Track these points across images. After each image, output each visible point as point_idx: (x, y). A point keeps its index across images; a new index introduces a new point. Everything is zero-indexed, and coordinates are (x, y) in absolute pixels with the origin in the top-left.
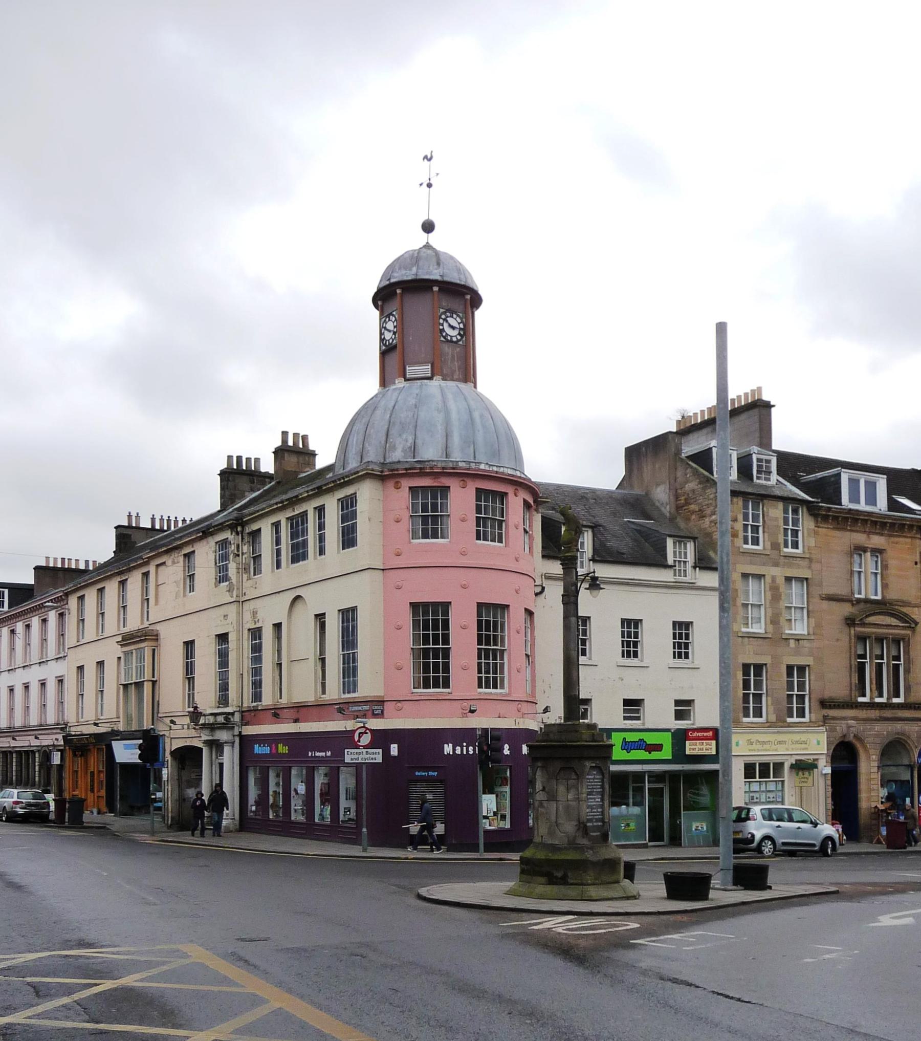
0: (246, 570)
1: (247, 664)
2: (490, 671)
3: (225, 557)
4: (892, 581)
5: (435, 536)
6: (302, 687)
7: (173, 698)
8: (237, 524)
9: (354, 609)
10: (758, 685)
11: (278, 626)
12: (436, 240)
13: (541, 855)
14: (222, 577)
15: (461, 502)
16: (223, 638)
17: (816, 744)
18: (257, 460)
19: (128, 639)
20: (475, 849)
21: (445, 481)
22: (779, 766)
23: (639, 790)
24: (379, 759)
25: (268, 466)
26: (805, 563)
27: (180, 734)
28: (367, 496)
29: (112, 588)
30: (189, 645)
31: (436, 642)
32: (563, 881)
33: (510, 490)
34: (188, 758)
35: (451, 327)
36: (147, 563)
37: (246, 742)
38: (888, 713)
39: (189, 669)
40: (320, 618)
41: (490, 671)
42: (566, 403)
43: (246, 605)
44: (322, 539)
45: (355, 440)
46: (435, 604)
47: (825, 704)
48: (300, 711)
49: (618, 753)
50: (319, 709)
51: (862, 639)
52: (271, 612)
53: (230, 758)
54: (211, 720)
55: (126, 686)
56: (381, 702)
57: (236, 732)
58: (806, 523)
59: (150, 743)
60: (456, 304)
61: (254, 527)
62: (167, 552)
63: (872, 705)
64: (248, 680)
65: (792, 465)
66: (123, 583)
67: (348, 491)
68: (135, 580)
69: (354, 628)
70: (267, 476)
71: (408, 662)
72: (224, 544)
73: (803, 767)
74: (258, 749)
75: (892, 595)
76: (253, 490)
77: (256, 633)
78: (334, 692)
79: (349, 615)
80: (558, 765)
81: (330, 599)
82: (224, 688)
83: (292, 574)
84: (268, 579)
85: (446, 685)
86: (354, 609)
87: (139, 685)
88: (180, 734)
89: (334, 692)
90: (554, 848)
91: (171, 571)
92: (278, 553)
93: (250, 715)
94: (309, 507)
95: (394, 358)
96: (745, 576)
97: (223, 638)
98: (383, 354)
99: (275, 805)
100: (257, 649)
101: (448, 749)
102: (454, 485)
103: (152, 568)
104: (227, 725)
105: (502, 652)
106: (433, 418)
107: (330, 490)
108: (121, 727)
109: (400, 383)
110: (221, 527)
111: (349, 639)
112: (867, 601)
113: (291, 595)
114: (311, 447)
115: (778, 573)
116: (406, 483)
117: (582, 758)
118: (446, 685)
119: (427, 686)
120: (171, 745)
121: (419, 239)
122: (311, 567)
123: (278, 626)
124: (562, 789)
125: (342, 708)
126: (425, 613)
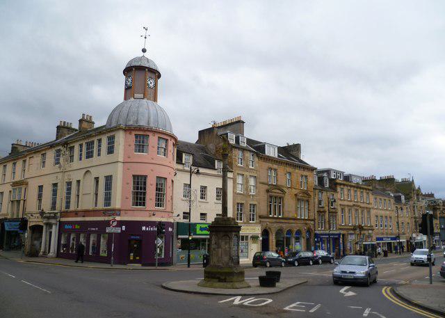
0: (67, 161)
1: (65, 195)
2: (159, 201)
3: (58, 156)
4: (279, 179)
5: (143, 152)
6: (87, 203)
7: (32, 206)
8: (65, 144)
9: (111, 176)
10: (241, 210)
11: (78, 182)
12: (146, 55)
13: (214, 270)
14: (57, 162)
15: (153, 140)
16: (55, 185)
17: (257, 230)
18: (91, 117)
19: (15, 184)
20: (154, 265)
21: (148, 133)
22: (247, 237)
23: (204, 245)
24: (119, 231)
25: (76, 126)
26: (255, 172)
27: (33, 221)
28: (120, 138)
29: (10, 166)
30: (41, 188)
31: (141, 189)
32: (225, 281)
33: (169, 138)
34: (37, 230)
35: (151, 83)
36: (26, 157)
37: (61, 224)
38: (278, 221)
39: (40, 196)
40: (97, 179)
41: (159, 201)
42: (184, 111)
43: (66, 174)
44: (99, 150)
45: (115, 116)
46: (141, 176)
47: (260, 217)
48: (86, 213)
49: (198, 232)
50: (95, 212)
51: (271, 197)
52: (75, 177)
53: (55, 230)
54: (48, 215)
55: (12, 201)
56: (120, 210)
57: (58, 220)
58: (256, 159)
59: (24, 222)
60: (153, 76)
61: (71, 145)
62: (34, 153)
63: (273, 218)
64: (64, 201)
65: (250, 142)
66: (14, 164)
67: (112, 134)
68: (19, 163)
69: (111, 183)
70: (76, 130)
71: (131, 197)
72: (59, 151)
73: (254, 238)
74: (66, 227)
75: (279, 183)
76: (68, 134)
77: (69, 184)
78: (101, 206)
79: (109, 179)
80: (222, 234)
81: (102, 173)
82: (54, 203)
83: (86, 163)
84: (76, 164)
85: (144, 205)
86: (111, 176)
87: (18, 202)
88: (33, 221)
89: (101, 206)
90: (218, 267)
91: (37, 159)
92: (81, 155)
93: (64, 214)
94: (95, 140)
95: (128, 91)
96: (238, 174)
97: (55, 185)
98: (126, 89)
99: (72, 248)
100: (69, 189)
101: (144, 228)
102: (151, 135)
103: (28, 159)
104: (55, 217)
105: (164, 194)
106: (144, 111)
107: (104, 133)
108: (9, 217)
109: (132, 99)
110: (58, 144)
111: (108, 186)
112: (272, 185)
113: (85, 170)
114: (93, 120)
115: (246, 174)
116: (134, 133)
117: (231, 231)
118: (144, 205)
119: (137, 205)
120: (30, 224)
121: (142, 54)
122: (95, 160)
123: (78, 182)
124: (223, 243)
125: (105, 212)
126: (138, 179)
